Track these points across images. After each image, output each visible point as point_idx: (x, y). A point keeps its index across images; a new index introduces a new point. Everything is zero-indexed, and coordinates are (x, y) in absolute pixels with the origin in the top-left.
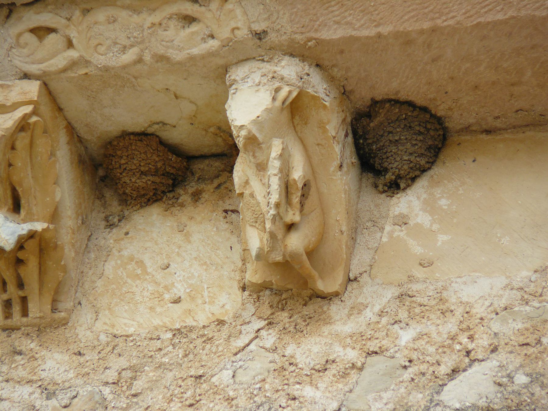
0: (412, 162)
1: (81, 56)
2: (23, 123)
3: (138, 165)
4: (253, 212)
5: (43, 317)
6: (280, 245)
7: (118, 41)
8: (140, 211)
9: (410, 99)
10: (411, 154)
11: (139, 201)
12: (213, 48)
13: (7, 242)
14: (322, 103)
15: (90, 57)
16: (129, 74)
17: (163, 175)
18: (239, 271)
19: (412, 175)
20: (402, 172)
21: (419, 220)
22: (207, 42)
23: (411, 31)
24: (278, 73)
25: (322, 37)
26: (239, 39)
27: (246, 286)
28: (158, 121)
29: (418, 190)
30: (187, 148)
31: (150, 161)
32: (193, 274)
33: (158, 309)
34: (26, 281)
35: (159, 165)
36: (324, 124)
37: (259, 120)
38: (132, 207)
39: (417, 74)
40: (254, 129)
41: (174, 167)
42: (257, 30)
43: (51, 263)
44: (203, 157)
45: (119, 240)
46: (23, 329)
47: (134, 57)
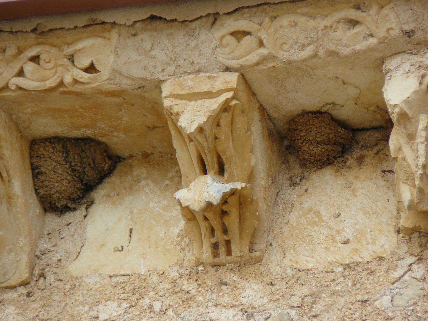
1: (270, 53)
2: (226, 105)
3: (315, 136)
5: (243, 256)
7: (298, 41)
8: (317, 172)
12: (373, 45)
13: (215, 198)
16: (307, 66)
17: (334, 144)
26: (393, 37)
27: (401, 230)
28: (330, 102)
31: (324, 133)
33: (332, 249)
34: (229, 228)
37: (409, 100)
41: (342, 138)
43: (248, 214)
44: (365, 129)
45: (300, 195)
46: (228, 265)
47: (311, 53)
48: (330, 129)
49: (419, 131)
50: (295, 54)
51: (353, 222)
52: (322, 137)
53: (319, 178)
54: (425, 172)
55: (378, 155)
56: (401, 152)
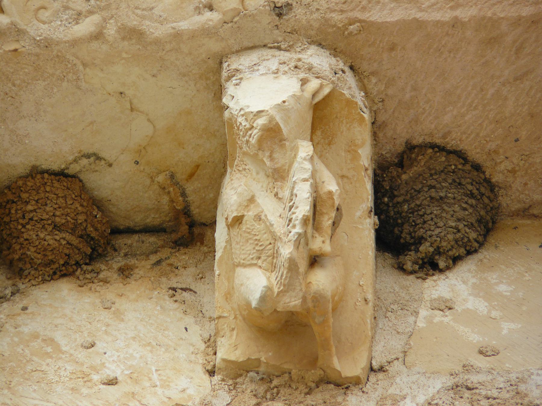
0: (459, 231)
1: (12, 23)
3: (52, 214)
4: (256, 242)
6: (301, 281)
7: (71, 5)
8: (41, 286)
9: (461, 147)
10: (459, 220)
11: (41, 272)
12: (211, 23)
14: (359, 113)
15: (27, 25)
16: (77, 58)
17: (81, 237)
18: (202, 354)
19: (455, 252)
20: (444, 244)
21: (470, 305)
22: (203, 14)
23: (503, 18)
24: (303, 60)
25: (371, 19)
26: (251, 11)
27: (216, 369)
28: (91, 151)
29: (463, 275)
30: (114, 210)
31: (69, 210)
32: (132, 355)
33: (85, 391)
35: (81, 218)
36: (356, 146)
37: (285, 106)
38: (29, 281)
39: (486, 101)
40: (278, 117)
41: (96, 230)
42: (278, 2)
44: (130, 231)
45: (14, 315)
47: (92, 29)
48: (82, 205)
49: (298, 159)
50: (61, 28)
51: (122, 356)
52: (64, 217)
53: (47, 293)
54: (305, 232)
55: (159, 267)
56: (252, 206)
